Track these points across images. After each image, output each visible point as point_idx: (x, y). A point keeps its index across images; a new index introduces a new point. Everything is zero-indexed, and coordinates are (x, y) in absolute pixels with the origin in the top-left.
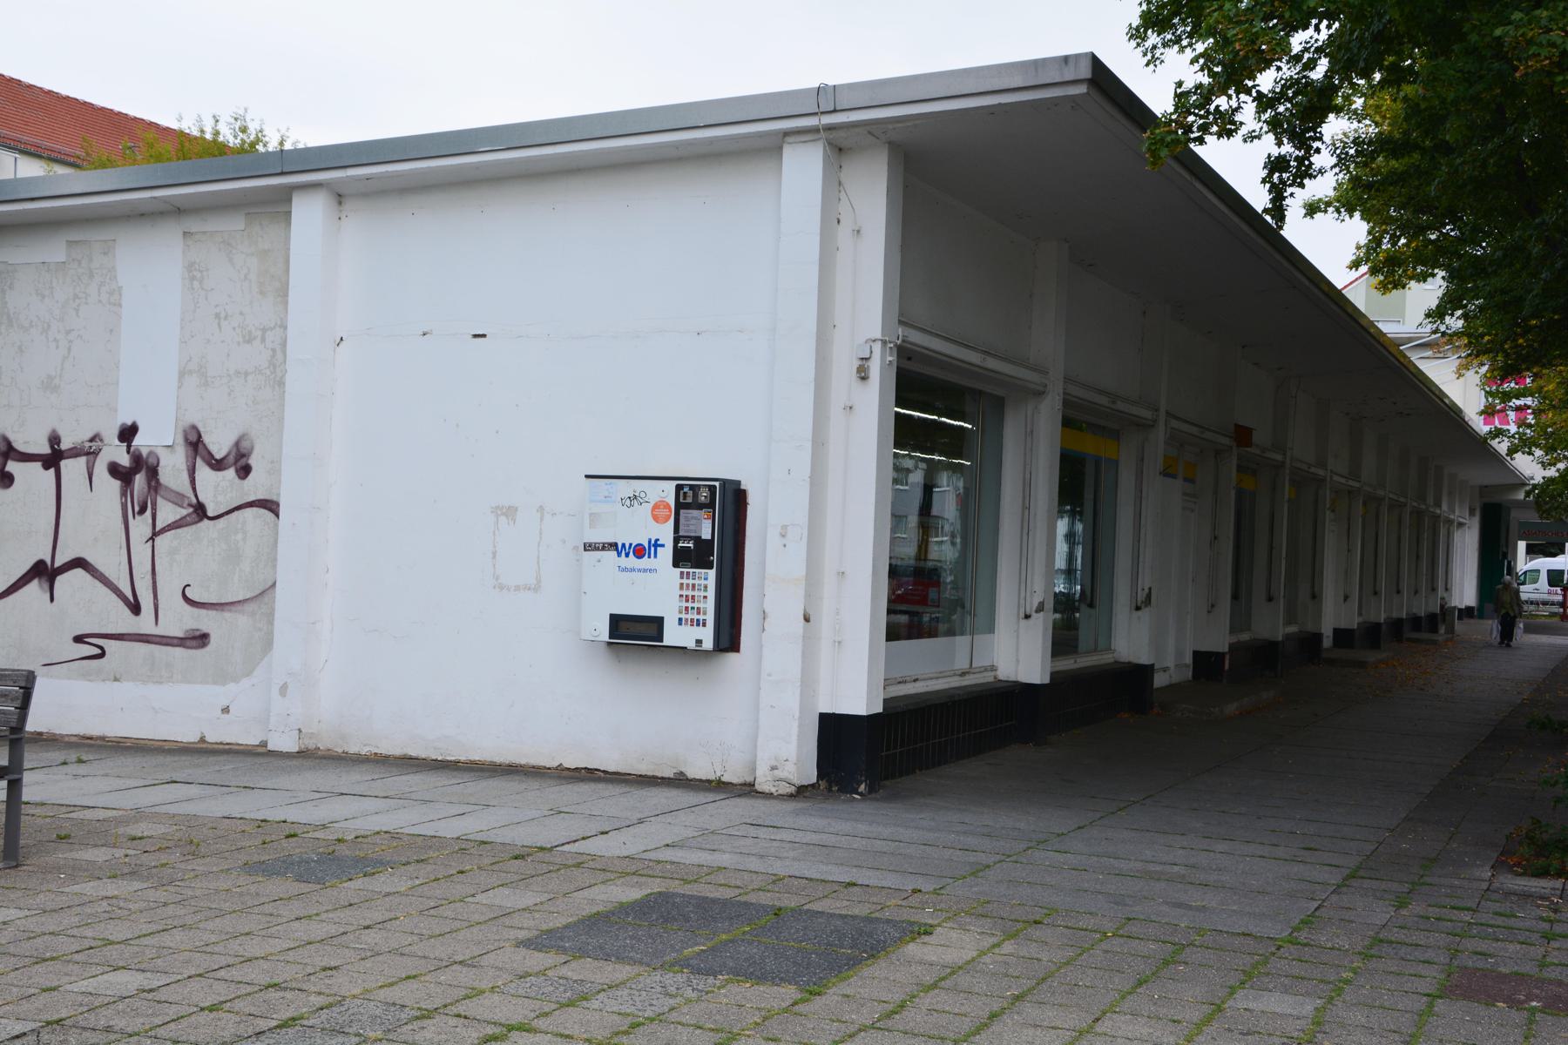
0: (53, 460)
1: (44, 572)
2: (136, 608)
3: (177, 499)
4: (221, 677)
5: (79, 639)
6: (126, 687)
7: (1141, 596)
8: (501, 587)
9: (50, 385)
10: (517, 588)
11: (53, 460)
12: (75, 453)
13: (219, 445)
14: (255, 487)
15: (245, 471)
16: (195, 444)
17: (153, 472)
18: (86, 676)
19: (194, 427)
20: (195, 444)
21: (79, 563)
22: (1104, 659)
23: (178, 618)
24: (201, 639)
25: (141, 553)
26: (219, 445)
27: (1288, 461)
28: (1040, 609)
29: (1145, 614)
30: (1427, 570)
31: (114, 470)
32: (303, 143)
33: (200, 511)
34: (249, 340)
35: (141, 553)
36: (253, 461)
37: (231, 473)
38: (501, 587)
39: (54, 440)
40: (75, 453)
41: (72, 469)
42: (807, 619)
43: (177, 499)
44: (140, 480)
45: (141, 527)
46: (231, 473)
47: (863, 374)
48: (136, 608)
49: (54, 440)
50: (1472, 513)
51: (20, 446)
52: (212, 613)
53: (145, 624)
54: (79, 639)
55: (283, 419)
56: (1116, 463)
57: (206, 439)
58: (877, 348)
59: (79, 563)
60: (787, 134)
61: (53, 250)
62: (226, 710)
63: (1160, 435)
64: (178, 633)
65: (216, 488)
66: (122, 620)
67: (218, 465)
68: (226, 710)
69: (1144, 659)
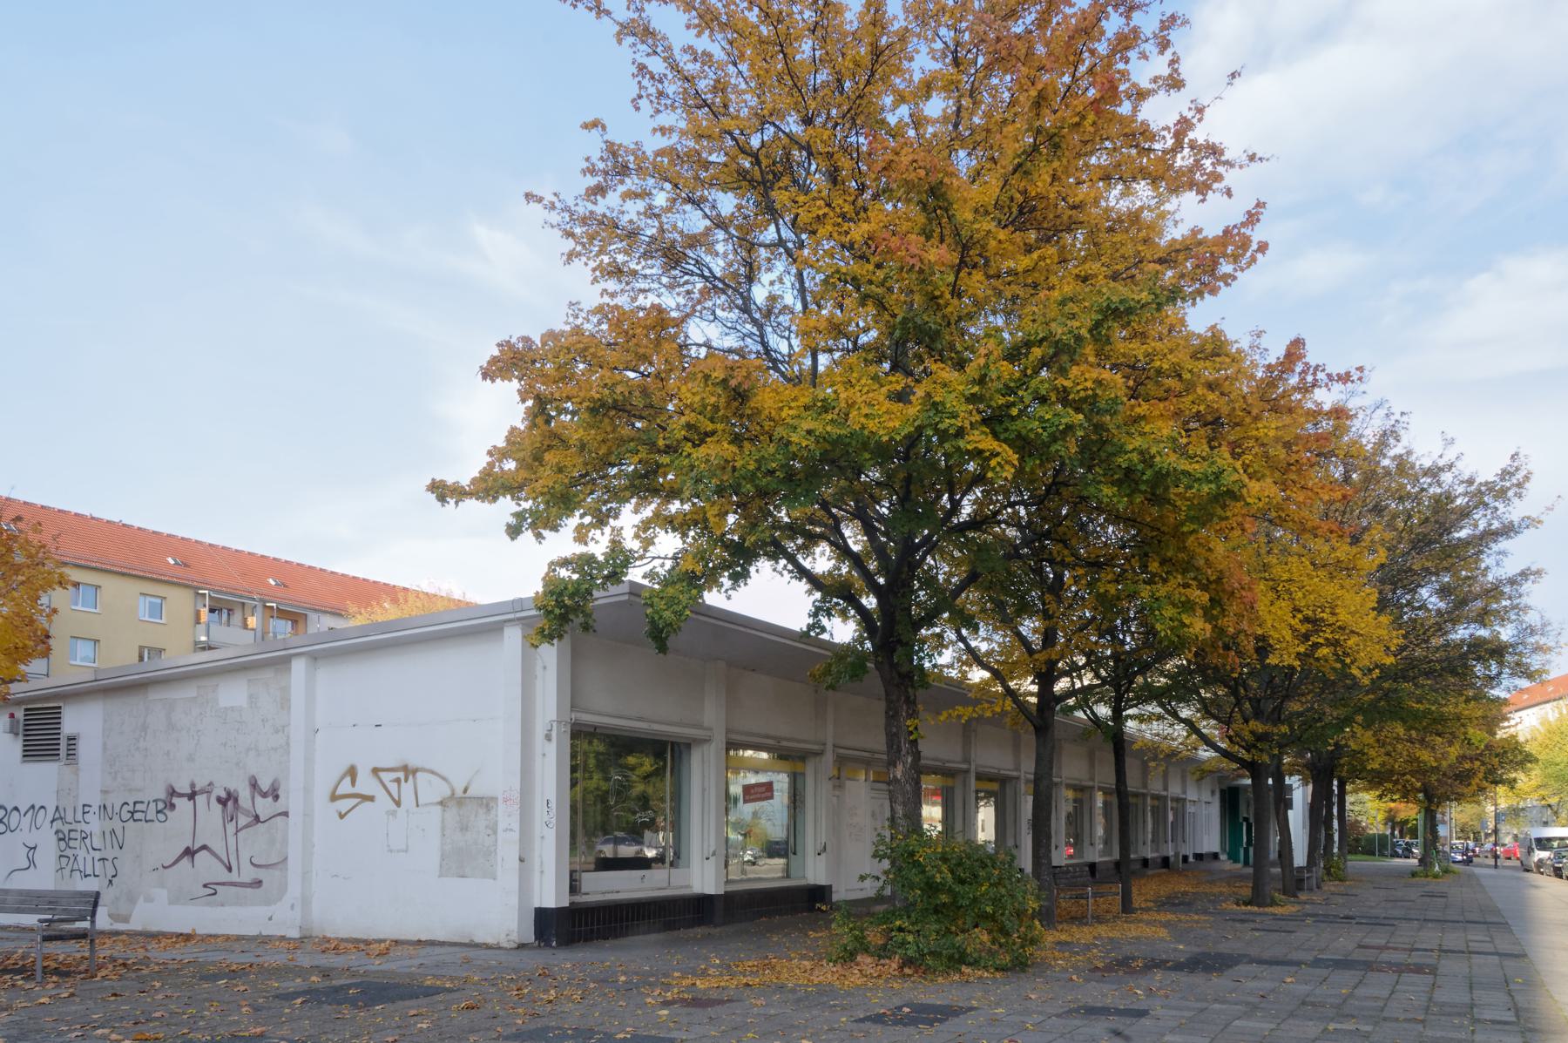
0: (192, 796)
1: (189, 853)
2: (230, 869)
3: (247, 813)
4: (268, 902)
5: (205, 886)
6: (227, 909)
7: (819, 848)
8: (391, 851)
9: (191, 759)
10: (398, 851)
11: (192, 796)
12: (202, 792)
13: (265, 785)
14: (280, 806)
15: (276, 797)
16: (254, 785)
17: (236, 800)
18: (208, 904)
19: (253, 777)
20: (254, 785)
21: (204, 847)
22: (802, 883)
23: (248, 874)
24: (258, 883)
25: (232, 840)
26: (265, 785)
27: (973, 767)
28: (714, 854)
29: (823, 855)
30: (1108, 830)
31: (219, 800)
32: (812, 598)
33: (257, 818)
34: (277, 732)
35: (232, 840)
36: (280, 792)
37: (270, 799)
38: (391, 851)
39: (193, 785)
40: (202, 792)
41: (200, 799)
42: (521, 860)
43: (247, 813)
44: (230, 804)
45: (231, 828)
46: (270, 799)
47: (548, 738)
48: (230, 869)
49: (193, 785)
50: (1213, 793)
51: (178, 790)
52: (263, 870)
53: (234, 877)
54: (205, 886)
55: (574, 769)
56: (803, 774)
57: (259, 782)
58: (555, 724)
59: (204, 847)
60: (505, 621)
61: (189, 691)
62: (270, 919)
63: (829, 757)
64: (248, 880)
65: (264, 806)
66: (224, 876)
67: (264, 795)
68: (270, 919)
69: (821, 880)
